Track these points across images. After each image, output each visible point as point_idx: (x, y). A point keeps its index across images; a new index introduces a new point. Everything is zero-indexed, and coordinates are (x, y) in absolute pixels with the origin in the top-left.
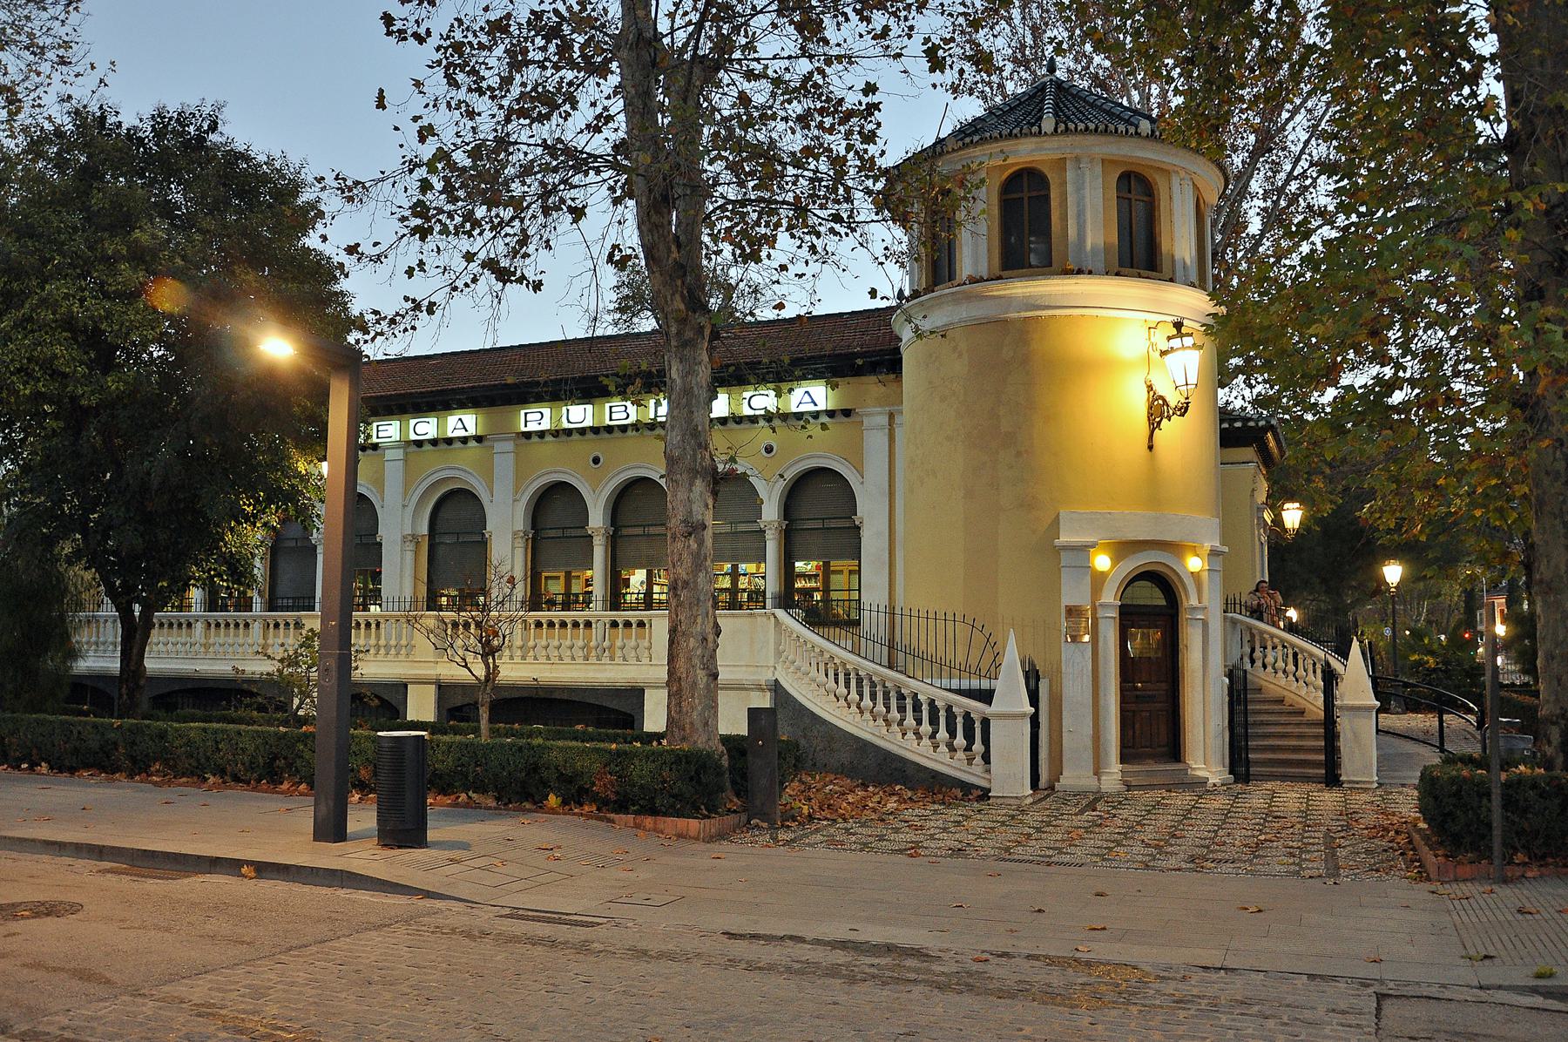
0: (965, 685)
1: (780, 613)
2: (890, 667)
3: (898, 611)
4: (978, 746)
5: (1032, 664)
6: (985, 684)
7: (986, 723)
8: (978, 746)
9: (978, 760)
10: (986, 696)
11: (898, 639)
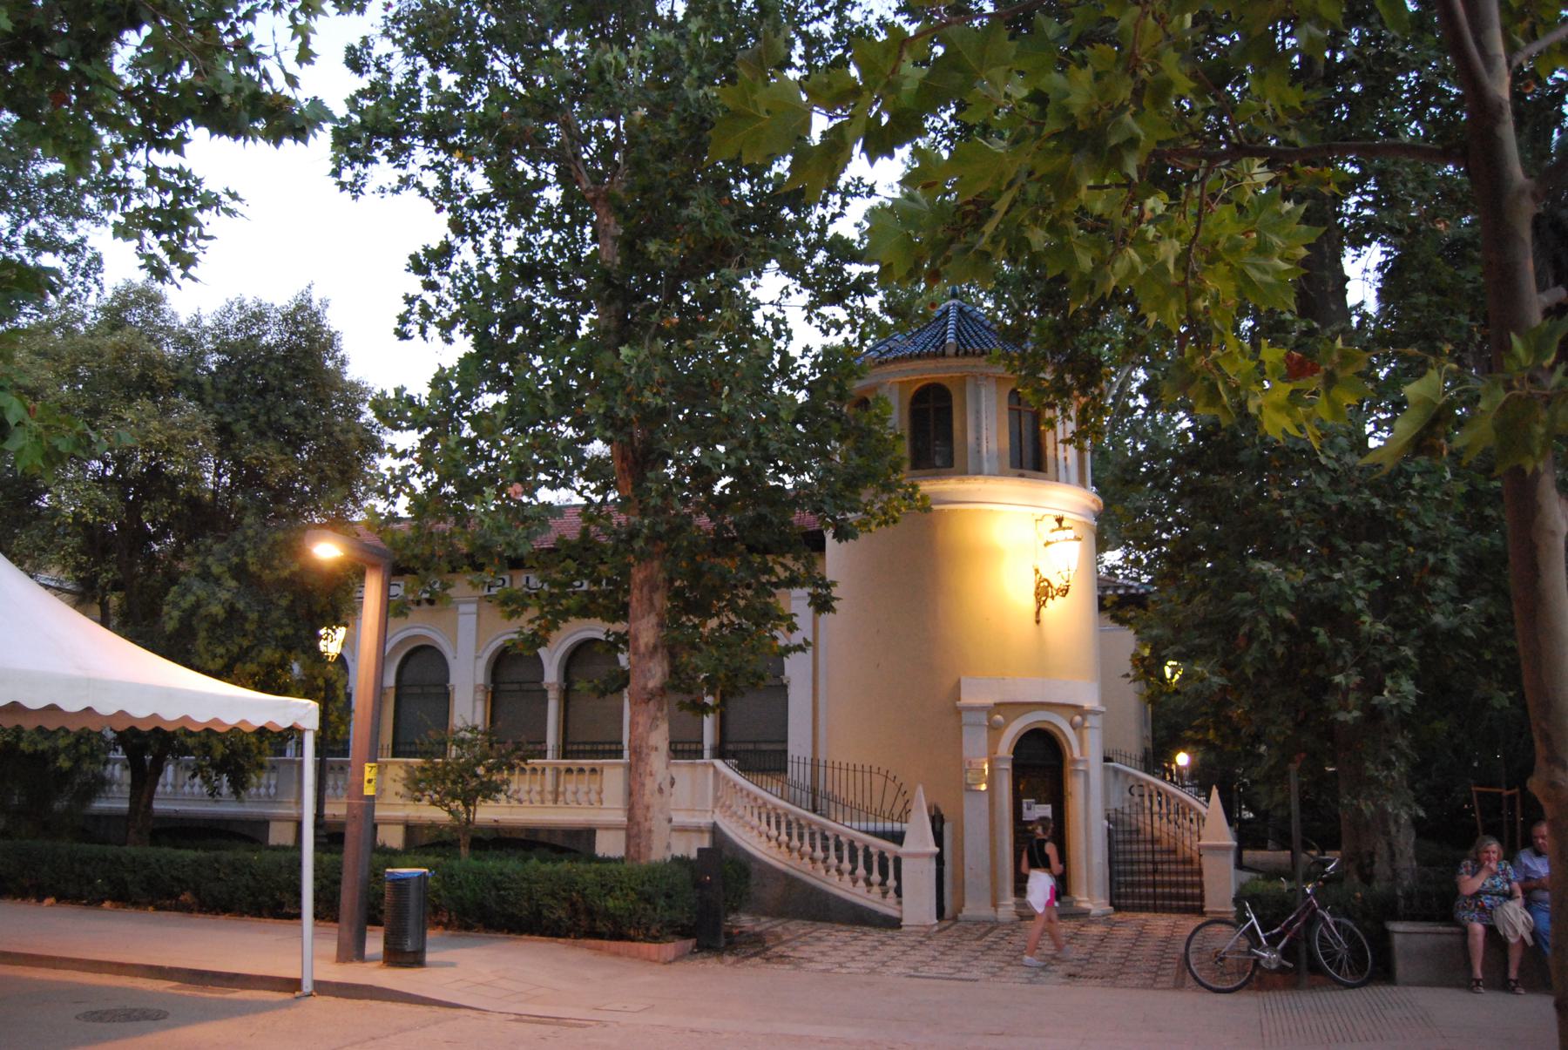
0: (880, 826)
1: (718, 763)
2: (814, 811)
3: (822, 763)
4: (891, 882)
5: (937, 809)
6: (897, 826)
7: (898, 861)
8: (891, 882)
9: (892, 893)
10: (898, 838)
11: (821, 788)
